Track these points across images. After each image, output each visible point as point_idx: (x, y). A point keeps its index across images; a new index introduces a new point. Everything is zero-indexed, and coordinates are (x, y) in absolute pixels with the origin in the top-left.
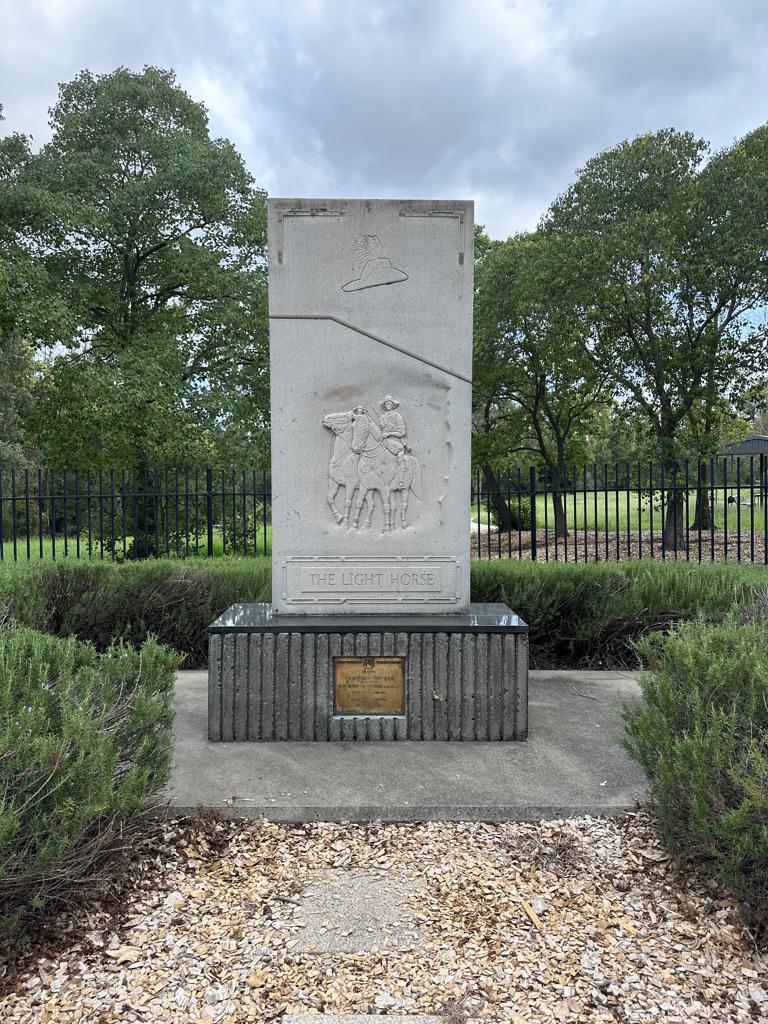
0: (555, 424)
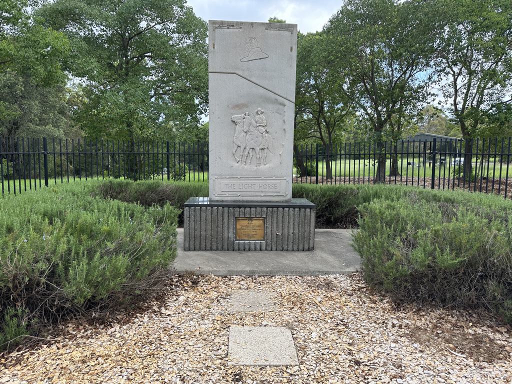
0: (328, 125)
